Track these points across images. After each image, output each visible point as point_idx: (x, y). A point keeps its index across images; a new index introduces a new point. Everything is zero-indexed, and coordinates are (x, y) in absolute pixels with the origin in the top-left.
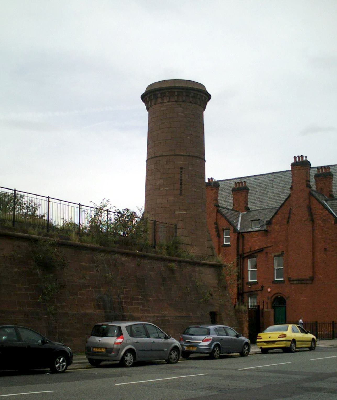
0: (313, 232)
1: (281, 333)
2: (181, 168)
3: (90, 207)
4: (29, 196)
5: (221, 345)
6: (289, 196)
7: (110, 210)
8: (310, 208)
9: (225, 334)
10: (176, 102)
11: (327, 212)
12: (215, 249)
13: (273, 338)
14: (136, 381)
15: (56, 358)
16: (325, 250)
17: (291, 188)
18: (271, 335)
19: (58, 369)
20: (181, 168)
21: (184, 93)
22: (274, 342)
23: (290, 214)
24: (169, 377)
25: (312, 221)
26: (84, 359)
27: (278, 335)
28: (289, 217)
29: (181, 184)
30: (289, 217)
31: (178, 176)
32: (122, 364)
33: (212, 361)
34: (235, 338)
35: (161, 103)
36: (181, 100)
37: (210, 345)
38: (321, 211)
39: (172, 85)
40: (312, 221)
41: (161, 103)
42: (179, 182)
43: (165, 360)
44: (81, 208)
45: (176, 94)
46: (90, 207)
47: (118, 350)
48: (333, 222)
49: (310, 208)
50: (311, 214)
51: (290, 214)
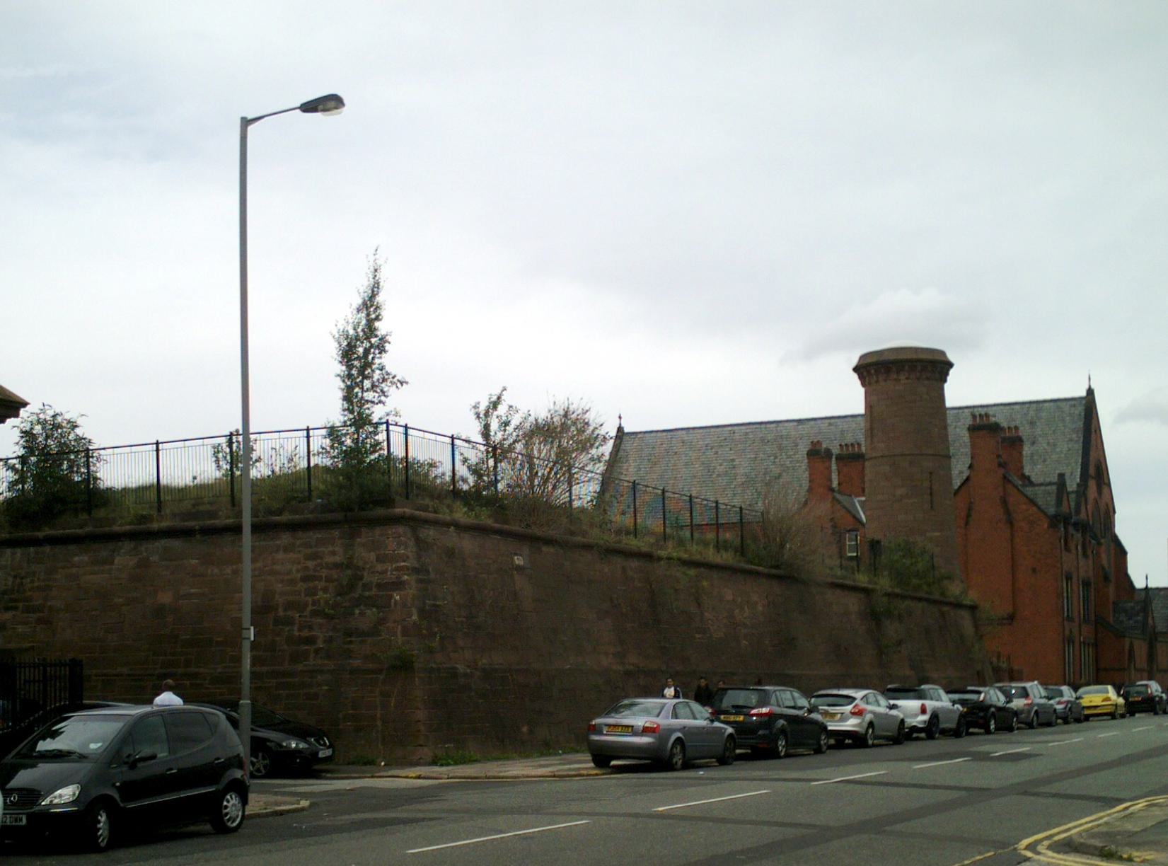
0: (1012, 541)
1: (1105, 696)
2: (931, 473)
3: (424, 431)
4: (438, 439)
5: (683, 737)
6: (968, 479)
7: (392, 419)
8: (1004, 502)
9: (691, 716)
10: (918, 379)
11: (1034, 508)
12: (255, 451)
13: (1095, 702)
14: (456, 842)
15: (226, 795)
16: (1034, 570)
17: (970, 467)
18: (1093, 699)
19: (229, 824)
20: (931, 473)
21: (930, 369)
22: (1096, 707)
23: (970, 509)
24: (739, 794)
25: (1010, 523)
26: (585, 762)
27: (1101, 699)
28: (968, 516)
29: (931, 494)
30: (968, 516)
31: (927, 484)
32: (1030, 726)
33: (862, 750)
34: (167, 756)
35: (895, 380)
36: (924, 377)
37: (1065, 708)
38: (1024, 507)
39: (914, 356)
40: (1010, 523)
41: (895, 380)
42: (929, 491)
43: (714, 760)
44: (409, 433)
45: (919, 368)
46: (424, 431)
47: (1029, 712)
48: (1046, 526)
49: (1004, 502)
50: (1008, 512)
51: (970, 509)
